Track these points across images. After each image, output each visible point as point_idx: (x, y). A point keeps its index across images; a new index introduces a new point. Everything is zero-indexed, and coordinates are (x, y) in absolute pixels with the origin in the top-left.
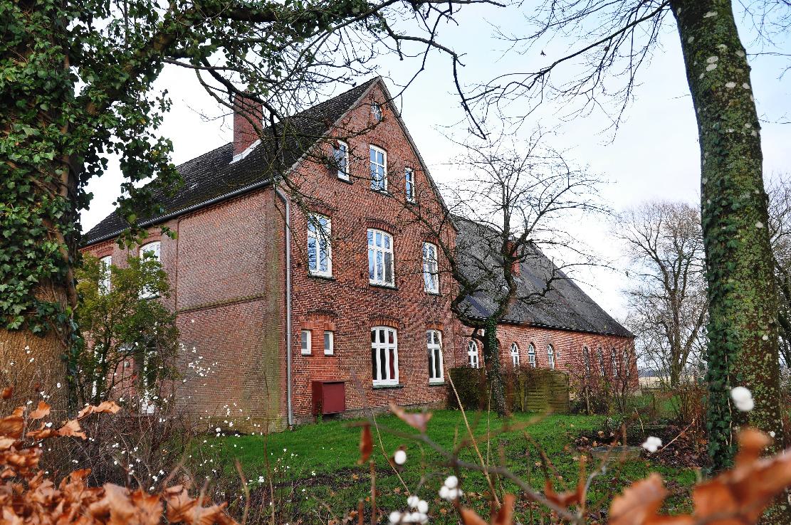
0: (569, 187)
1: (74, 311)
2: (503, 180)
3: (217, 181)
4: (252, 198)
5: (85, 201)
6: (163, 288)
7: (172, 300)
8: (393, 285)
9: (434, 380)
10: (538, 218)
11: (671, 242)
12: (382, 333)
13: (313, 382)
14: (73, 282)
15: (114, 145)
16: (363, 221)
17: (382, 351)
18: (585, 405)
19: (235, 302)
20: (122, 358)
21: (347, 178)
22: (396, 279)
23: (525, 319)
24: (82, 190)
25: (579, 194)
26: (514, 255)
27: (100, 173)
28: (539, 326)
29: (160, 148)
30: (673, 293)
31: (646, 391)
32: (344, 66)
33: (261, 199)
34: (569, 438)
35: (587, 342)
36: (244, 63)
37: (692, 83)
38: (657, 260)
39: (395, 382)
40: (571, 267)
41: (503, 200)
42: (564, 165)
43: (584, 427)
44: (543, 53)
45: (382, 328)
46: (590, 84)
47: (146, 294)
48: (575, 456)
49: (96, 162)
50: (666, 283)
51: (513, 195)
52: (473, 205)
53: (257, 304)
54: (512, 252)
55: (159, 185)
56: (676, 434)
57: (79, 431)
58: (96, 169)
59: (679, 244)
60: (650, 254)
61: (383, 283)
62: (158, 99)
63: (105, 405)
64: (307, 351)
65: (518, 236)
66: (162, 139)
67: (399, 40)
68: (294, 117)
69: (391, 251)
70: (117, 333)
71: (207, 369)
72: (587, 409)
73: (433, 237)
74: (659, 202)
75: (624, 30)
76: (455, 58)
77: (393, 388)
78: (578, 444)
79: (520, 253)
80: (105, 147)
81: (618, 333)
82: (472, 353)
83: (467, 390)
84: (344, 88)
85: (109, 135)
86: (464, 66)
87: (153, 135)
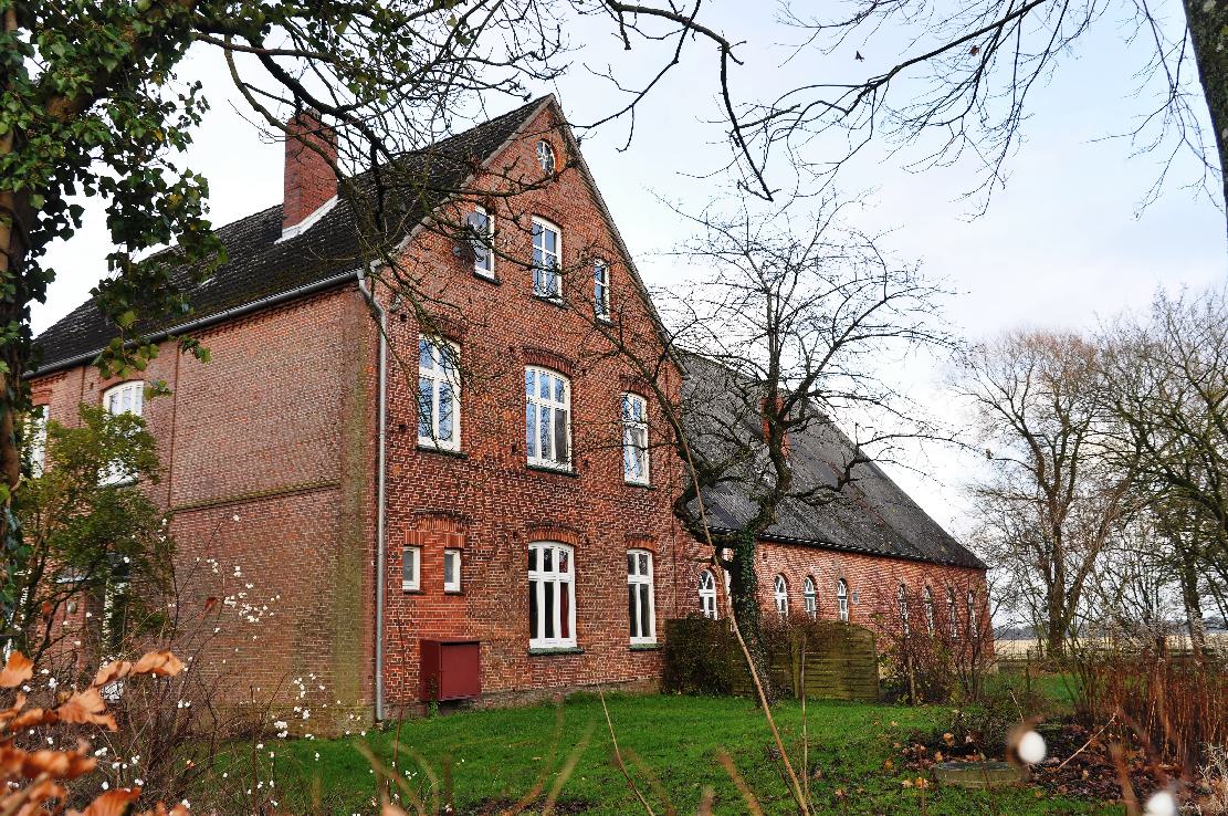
0: (886, 299)
1: (12, 494)
2: (769, 284)
3: (256, 273)
4: (301, 311)
5: (38, 284)
6: (147, 465)
7: (162, 489)
8: (569, 467)
9: (638, 640)
10: (831, 353)
11: (1050, 402)
12: (548, 553)
13: (423, 642)
14: (12, 435)
15: (97, 180)
16: (518, 353)
17: (549, 587)
18: (906, 688)
19: (283, 494)
20: (63, 596)
21: (490, 275)
22: (573, 456)
23: (802, 533)
24: (35, 264)
25: (900, 313)
26: (787, 418)
27: (67, 234)
28: (820, 546)
29: (183, 190)
30: (1052, 492)
31: (1008, 665)
32: (508, 64)
33: (333, 308)
34: (891, 746)
35: (909, 575)
36: (341, 40)
37: (1211, 85)
38: (1025, 433)
39: (570, 643)
40: (889, 440)
41: (769, 316)
42: (878, 260)
43: (910, 725)
44: (858, 56)
45: (548, 545)
46: (961, 106)
47: (114, 475)
48: (906, 778)
49: (61, 211)
50: (1039, 473)
51: (788, 310)
52: (715, 326)
53: (324, 497)
54: (784, 412)
55: (181, 260)
56: (1080, 740)
57: (101, 713)
58: (60, 226)
59: (1063, 407)
60: (1013, 422)
61: (553, 465)
62: (181, 97)
63: (152, 660)
64: (414, 584)
65: (794, 386)
66: (188, 174)
67: (623, 13)
68: (411, 153)
69: (566, 406)
70: (57, 550)
71: (261, 606)
72: (910, 694)
73: (643, 383)
74: (1030, 333)
75: (1001, 24)
76: (725, 48)
77: (565, 653)
78: (909, 756)
79: (796, 416)
80: (78, 185)
81: (962, 562)
82: (707, 594)
83: (693, 661)
84: (515, 103)
85: (87, 161)
86: (741, 64)
87: (171, 166)
